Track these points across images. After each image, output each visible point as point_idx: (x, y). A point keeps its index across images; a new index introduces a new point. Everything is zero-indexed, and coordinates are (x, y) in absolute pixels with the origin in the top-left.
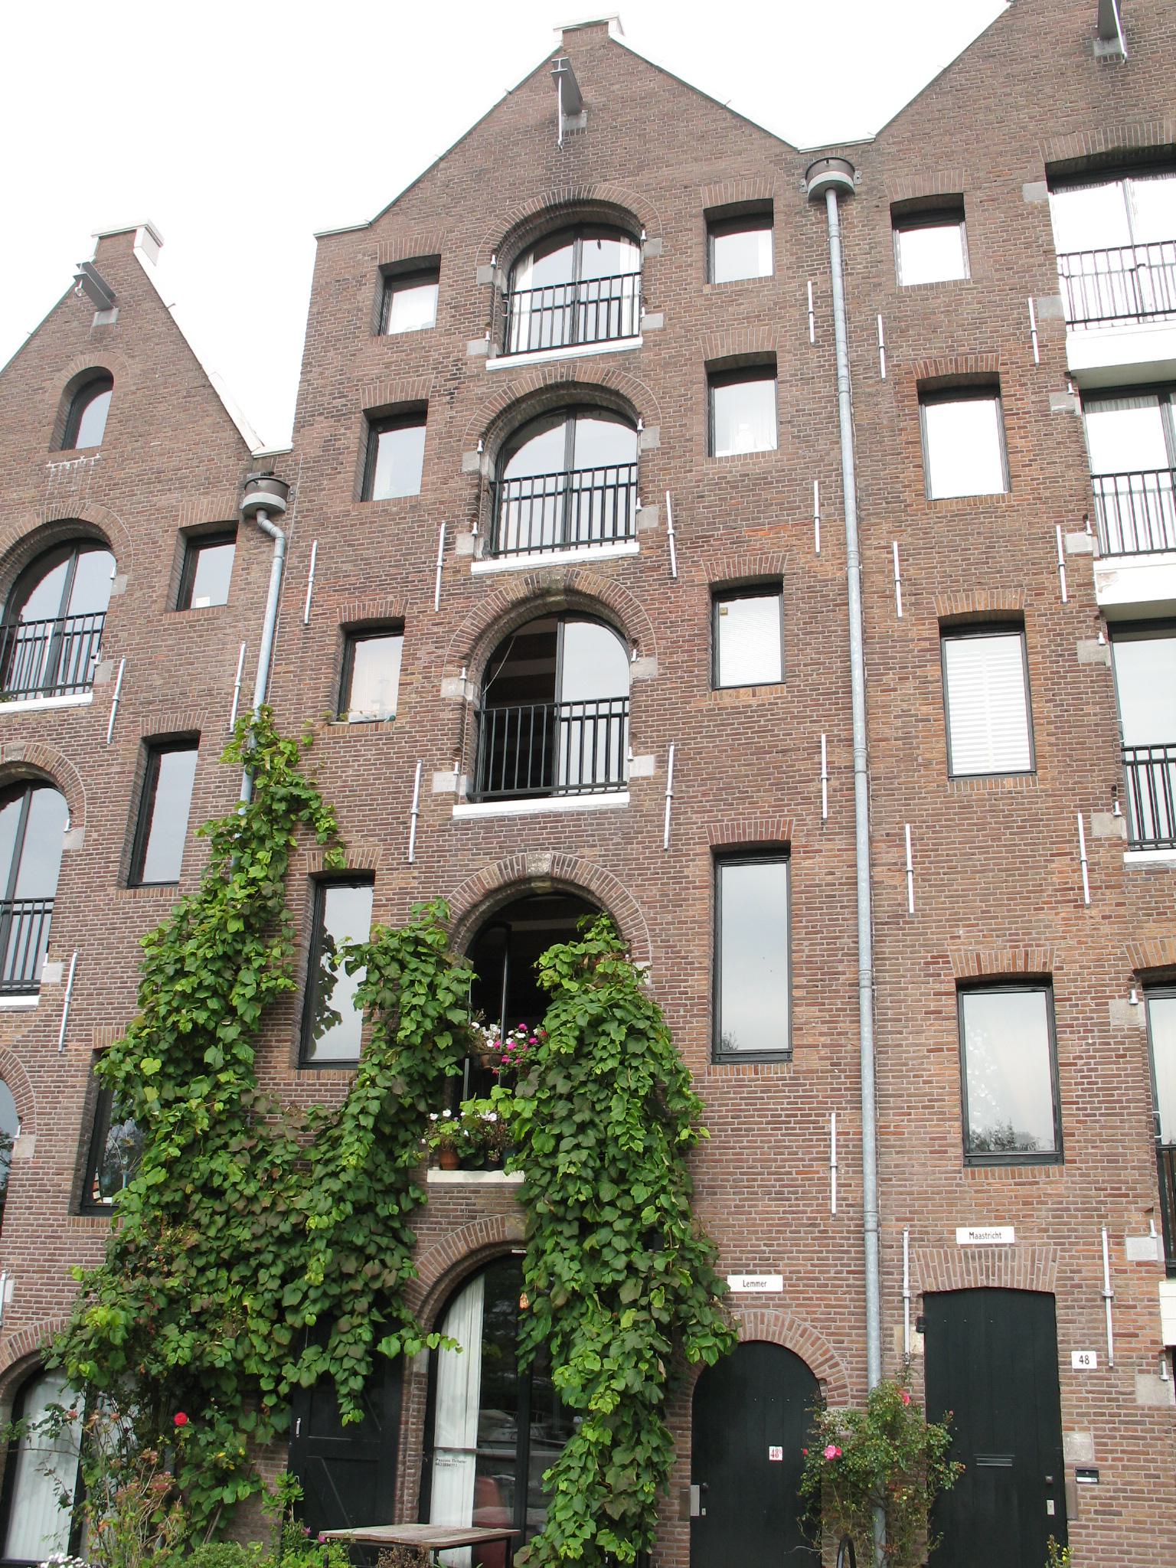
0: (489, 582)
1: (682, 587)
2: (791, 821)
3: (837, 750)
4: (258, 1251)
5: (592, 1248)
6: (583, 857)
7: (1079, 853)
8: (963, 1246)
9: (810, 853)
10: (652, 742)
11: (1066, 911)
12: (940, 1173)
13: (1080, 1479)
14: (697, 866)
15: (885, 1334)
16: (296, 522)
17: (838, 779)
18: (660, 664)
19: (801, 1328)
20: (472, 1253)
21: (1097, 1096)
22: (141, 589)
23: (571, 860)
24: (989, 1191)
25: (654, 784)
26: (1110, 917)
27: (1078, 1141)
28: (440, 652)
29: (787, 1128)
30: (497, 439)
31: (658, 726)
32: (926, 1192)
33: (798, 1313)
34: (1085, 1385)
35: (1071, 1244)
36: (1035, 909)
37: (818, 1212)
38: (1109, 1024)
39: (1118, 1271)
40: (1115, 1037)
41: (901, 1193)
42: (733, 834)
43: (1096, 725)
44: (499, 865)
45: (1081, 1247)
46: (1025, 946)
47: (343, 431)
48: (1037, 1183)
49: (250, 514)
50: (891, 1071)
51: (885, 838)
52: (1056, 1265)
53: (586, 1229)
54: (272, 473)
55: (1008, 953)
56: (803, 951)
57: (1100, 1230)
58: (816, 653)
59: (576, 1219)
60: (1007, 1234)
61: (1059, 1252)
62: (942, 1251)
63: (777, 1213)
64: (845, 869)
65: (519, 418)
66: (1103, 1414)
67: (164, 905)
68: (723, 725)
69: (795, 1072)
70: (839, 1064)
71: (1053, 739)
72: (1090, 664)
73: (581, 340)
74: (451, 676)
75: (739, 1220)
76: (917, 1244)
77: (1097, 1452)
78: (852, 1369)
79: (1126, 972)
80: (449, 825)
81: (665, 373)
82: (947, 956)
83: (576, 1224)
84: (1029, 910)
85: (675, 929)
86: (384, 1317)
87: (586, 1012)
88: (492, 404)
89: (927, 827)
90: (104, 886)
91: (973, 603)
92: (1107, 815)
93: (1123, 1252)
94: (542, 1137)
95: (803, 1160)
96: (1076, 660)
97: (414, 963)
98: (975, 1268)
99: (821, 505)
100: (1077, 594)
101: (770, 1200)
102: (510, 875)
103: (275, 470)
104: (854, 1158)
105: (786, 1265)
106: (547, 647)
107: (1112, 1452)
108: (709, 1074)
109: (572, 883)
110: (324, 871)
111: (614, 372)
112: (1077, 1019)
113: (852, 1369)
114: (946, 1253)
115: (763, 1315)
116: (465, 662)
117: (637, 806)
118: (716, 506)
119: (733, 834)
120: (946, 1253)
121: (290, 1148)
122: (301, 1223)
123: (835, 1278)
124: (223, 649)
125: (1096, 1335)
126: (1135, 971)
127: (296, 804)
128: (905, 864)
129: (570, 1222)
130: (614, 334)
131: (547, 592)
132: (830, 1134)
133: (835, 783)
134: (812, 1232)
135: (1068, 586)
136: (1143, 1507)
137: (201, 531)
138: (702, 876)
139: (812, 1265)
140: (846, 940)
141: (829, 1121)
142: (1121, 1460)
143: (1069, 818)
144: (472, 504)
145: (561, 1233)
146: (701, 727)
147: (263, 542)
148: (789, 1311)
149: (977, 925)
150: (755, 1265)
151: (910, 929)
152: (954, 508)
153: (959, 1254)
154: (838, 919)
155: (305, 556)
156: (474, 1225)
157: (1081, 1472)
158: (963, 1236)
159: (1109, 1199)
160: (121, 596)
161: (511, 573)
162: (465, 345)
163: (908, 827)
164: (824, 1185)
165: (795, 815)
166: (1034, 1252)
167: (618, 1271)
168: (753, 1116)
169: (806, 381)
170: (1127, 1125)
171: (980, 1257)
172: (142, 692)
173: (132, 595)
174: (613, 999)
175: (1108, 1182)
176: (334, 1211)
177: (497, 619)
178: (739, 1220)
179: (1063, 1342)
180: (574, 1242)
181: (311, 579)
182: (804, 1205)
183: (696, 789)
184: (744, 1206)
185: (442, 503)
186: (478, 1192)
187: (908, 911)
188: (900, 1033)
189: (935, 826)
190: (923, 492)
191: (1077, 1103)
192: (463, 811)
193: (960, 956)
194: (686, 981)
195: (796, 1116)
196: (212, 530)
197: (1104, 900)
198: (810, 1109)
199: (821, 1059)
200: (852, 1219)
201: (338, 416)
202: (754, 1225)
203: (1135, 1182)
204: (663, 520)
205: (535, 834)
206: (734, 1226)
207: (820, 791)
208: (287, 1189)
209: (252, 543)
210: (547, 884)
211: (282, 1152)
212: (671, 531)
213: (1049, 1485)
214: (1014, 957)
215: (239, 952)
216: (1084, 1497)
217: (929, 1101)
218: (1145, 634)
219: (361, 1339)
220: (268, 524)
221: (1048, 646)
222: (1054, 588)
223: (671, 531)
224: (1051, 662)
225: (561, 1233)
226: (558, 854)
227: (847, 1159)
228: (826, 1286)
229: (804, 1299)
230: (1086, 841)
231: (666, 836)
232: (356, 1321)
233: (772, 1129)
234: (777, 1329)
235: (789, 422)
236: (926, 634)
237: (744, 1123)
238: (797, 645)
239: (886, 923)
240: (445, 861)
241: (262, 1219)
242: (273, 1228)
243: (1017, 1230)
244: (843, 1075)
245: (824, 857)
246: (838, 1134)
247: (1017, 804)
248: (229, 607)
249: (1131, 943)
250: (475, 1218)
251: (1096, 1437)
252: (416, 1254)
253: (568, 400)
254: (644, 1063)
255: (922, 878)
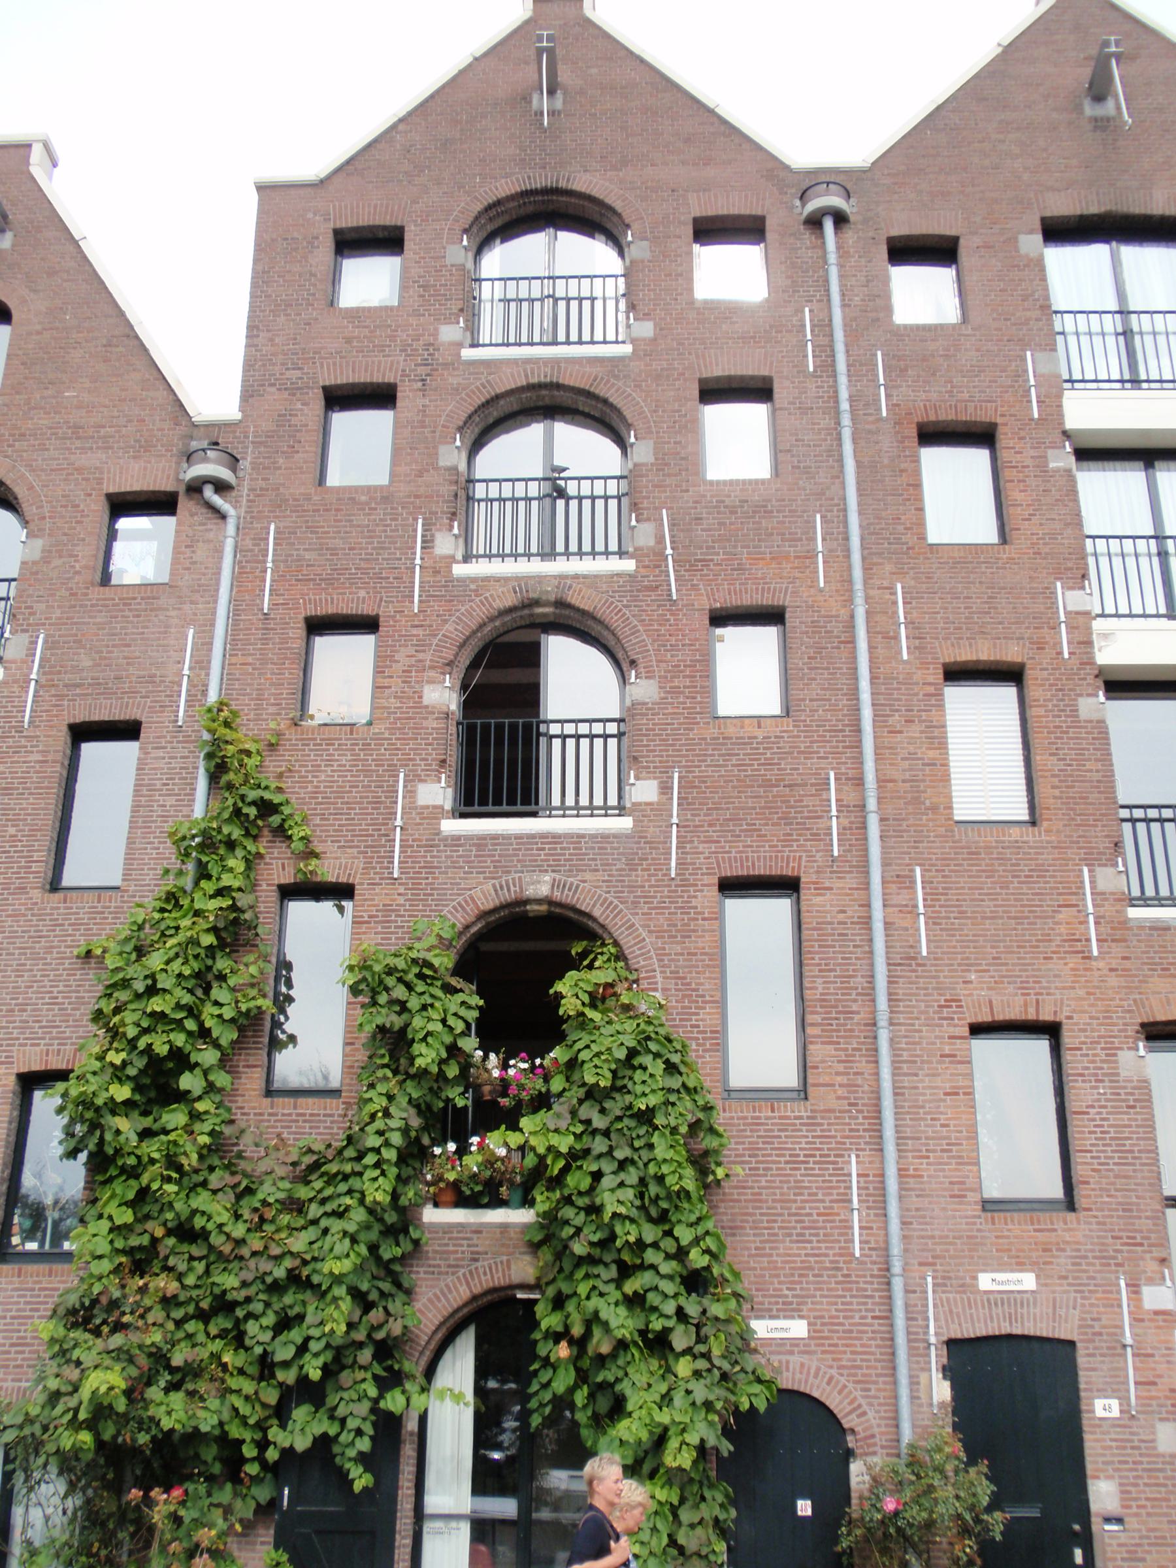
0: (473, 587)
1: (681, 610)
2: (800, 857)
3: (845, 788)
4: (248, 1300)
5: (635, 1293)
6: (584, 881)
7: (1085, 906)
8: (986, 1292)
9: (821, 889)
10: (655, 767)
11: (1074, 961)
12: (960, 1217)
13: (1107, 1527)
14: (705, 896)
15: (914, 1382)
16: (248, 501)
17: (847, 817)
18: (660, 687)
19: (828, 1376)
20: (475, 1298)
21: (1110, 1145)
22: (60, 557)
23: (572, 884)
24: (1008, 1237)
25: (659, 810)
26: (1116, 970)
27: (1093, 1190)
28: (421, 656)
29: (806, 1169)
30: (472, 433)
31: (661, 751)
32: (947, 1237)
33: (823, 1360)
34: (1109, 1433)
35: (1090, 1292)
36: (1045, 958)
37: (841, 1255)
38: (1118, 1074)
39: (1136, 1320)
40: (1125, 1088)
41: (923, 1237)
42: (742, 866)
43: (1098, 781)
44: (494, 886)
45: (1099, 1295)
46: (1036, 994)
47: (299, 406)
48: (1055, 1230)
49: (195, 488)
50: (908, 1113)
51: (898, 881)
52: (1077, 1312)
53: (625, 1271)
54: (216, 444)
55: (1019, 1000)
56: (816, 988)
57: (1118, 1278)
58: (823, 689)
59: (614, 1261)
60: (1027, 1281)
61: (1079, 1300)
62: (965, 1296)
63: (799, 1255)
64: (857, 908)
65: (495, 413)
66: (1126, 1462)
67: (103, 913)
68: (729, 755)
69: (812, 1111)
70: (856, 1105)
71: (1057, 792)
72: (1091, 721)
73: (524, 339)
74: (434, 682)
75: (759, 1262)
76: (939, 1289)
77: (1122, 1499)
78: (881, 1418)
79: (1133, 1024)
80: (437, 840)
81: (657, 385)
82: (960, 1001)
83: (614, 1267)
84: (1038, 958)
85: (685, 960)
86: (385, 1369)
87: (622, 1044)
88: (470, 397)
89: (937, 871)
90: (25, 888)
91: (977, 651)
92: (1110, 871)
93: (1140, 1300)
94: (578, 1174)
95: (823, 1201)
96: (1077, 716)
97: (420, 987)
98: (997, 1314)
99: (824, 539)
100: (1078, 651)
101: (791, 1242)
102: (507, 896)
103: (220, 441)
104: (877, 1198)
105: (810, 1310)
106: (531, 657)
107: (1136, 1499)
108: (724, 1111)
109: (574, 909)
110: (295, 883)
111: (602, 379)
112: (1087, 1068)
113: (881, 1418)
114: (969, 1299)
115: (788, 1362)
116: (448, 669)
117: (641, 831)
118: (715, 530)
119: (742, 866)
120: (969, 1299)
121: (281, 1184)
122: (297, 1268)
123: (860, 1324)
124: (166, 632)
125: (1119, 1383)
126: (1143, 1025)
127: (267, 808)
128: (916, 906)
129: (606, 1265)
130: (574, 337)
131: (536, 603)
132: (850, 1175)
133: (846, 822)
134: (835, 1276)
135: (1069, 643)
136: (1166, 1552)
137: (129, 498)
138: (711, 907)
139: (837, 1310)
140: (859, 979)
141: (849, 1162)
142: (1144, 1507)
143: (1074, 870)
144: (451, 502)
145: (598, 1276)
146: (705, 755)
147: (210, 519)
148: (814, 1357)
149: (988, 971)
150: (778, 1310)
151: (923, 971)
152: (956, 555)
153: (982, 1301)
154: (850, 958)
155: (261, 539)
156: (476, 1268)
157: (1108, 1520)
158: (986, 1281)
159: (1125, 1248)
160: (34, 563)
161: (498, 580)
162: (436, 330)
163: (918, 870)
164: (846, 1227)
165: (806, 851)
166: (1054, 1300)
167: (668, 1317)
168: (770, 1155)
169: (804, 410)
170: (1139, 1175)
171: (1003, 1304)
172: (66, 673)
173: (49, 562)
174: (644, 1032)
175: (1123, 1230)
176: (352, 1254)
177: (481, 626)
178: (759, 1262)
179: (1086, 1390)
180: (612, 1286)
181: (269, 565)
182: (827, 1248)
183: (702, 818)
184: (764, 1248)
185: (416, 497)
186: (479, 1232)
187: (920, 953)
188: (916, 1075)
189: (943, 871)
190: (923, 537)
191: (1090, 1151)
192: (452, 826)
193: (973, 1001)
194: (697, 1014)
195: (814, 1156)
196: (142, 499)
197: (1109, 953)
198: (829, 1149)
199: (839, 1098)
200: (875, 1263)
201: (293, 390)
202: (776, 1268)
203: (1149, 1231)
204: (660, 540)
205: (532, 855)
206: (755, 1269)
207: (830, 828)
208: (278, 1230)
209: (196, 518)
210: (544, 908)
211: (274, 1189)
212: (669, 551)
213: (1075, 1534)
214: (1026, 1005)
215: (209, 968)
216: (1110, 1545)
217: (948, 1144)
218: (1167, 694)
219: (366, 1395)
220: (217, 500)
221: (1051, 700)
222: (1055, 644)
223: (669, 551)
224: (1054, 716)
225: (598, 1276)
226: (558, 877)
227: (868, 1201)
228: (851, 1331)
229: (830, 1345)
230: (1092, 894)
231: (673, 864)
232: (360, 1375)
233: (791, 1169)
234: (804, 1377)
235: (789, 451)
236: (931, 679)
237: (762, 1162)
238: (802, 679)
239: (900, 964)
240: (434, 878)
241: (252, 1263)
242: (265, 1273)
243: (1038, 1277)
244: (860, 1116)
245: (835, 894)
246: (858, 1175)
247: (1024, 853)
248: (171, 587)
249: (1137, 997)
250: (476, 1260)
251: (1121, 1485)
252: (412, 1300)
253: (547, 401)
254: (679, 1099)
255: (932, 921)
